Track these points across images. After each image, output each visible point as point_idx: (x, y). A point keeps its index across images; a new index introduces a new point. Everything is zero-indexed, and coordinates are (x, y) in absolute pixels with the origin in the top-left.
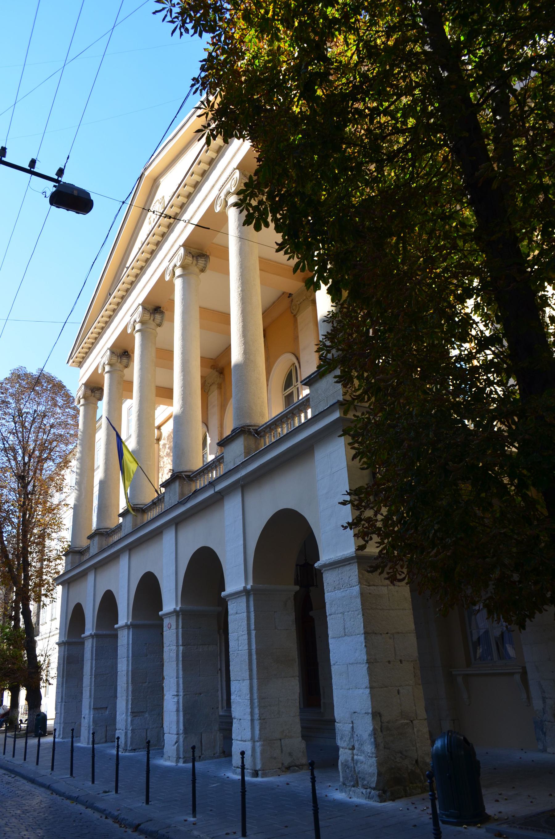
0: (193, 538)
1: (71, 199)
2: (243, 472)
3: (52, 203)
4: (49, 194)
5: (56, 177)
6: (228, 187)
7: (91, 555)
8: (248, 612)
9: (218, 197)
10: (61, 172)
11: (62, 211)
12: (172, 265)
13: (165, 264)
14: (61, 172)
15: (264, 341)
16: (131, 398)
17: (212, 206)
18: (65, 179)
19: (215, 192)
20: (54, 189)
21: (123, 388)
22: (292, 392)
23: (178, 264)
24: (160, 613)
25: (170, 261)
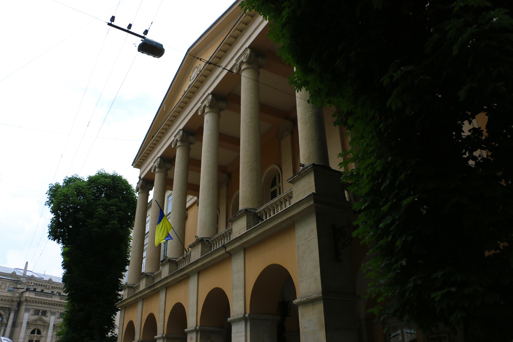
0: (209, 283)
1: (151, 48)
2: (200, 264)
3: (139, 51)
4: (138, 45)
5: (143, 35)
6: (205, 102)
7: (163, 277)
8: (246, 332)
9: (235, 65)
10: (146, 32)
11: (145, 56)
12: (203, 105)
13: (199, 105)
14: (146, 32)
15: (154, 241)
16: (172, 190)
17: (197, 111)
18: (148, 37)
19: (234, 62)
20: (142, 42)
21: (168, 184)
22: (276, 190)
23: (207, 105)
24: (186, 330)
25: (202, 103)
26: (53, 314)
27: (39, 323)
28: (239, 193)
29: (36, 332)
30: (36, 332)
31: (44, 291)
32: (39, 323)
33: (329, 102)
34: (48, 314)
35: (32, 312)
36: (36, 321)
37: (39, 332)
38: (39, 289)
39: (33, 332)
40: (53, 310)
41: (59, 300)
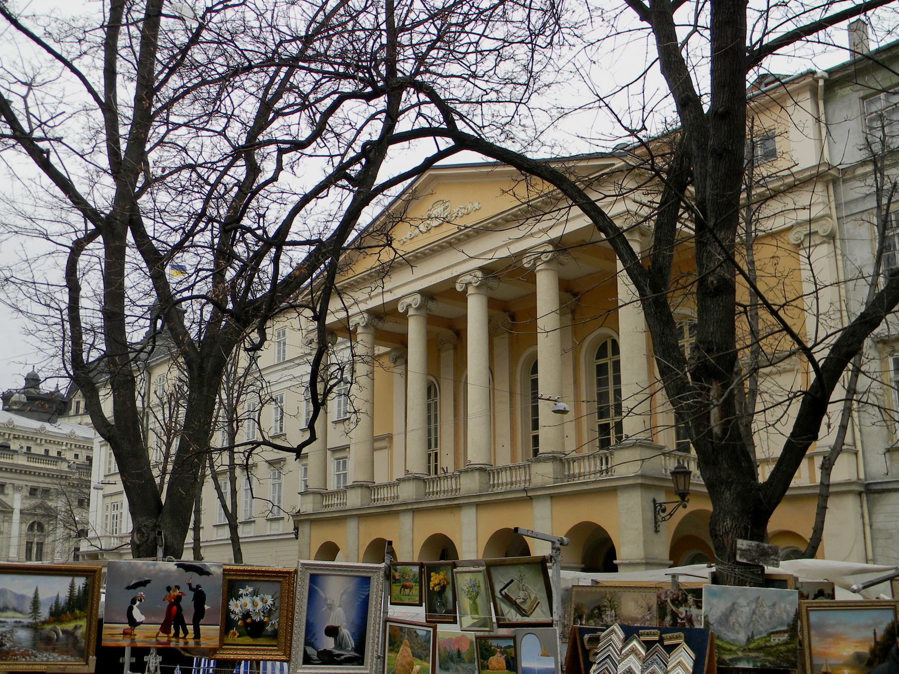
17: (524, 252)
26: (17, 489)
27: (39, 511)
28: (535, 354)
29: (36, 528)
30: (36, 528)
31: (33, 451)
32: (39, 511)
33: (771, 155)
34: (9, 490)
35: (26, 492)
36: (35, 508)
37: (41, 527)
38: (53, 453)
39: (31, 528)
40: (17, 483)
41: (26, 463)
